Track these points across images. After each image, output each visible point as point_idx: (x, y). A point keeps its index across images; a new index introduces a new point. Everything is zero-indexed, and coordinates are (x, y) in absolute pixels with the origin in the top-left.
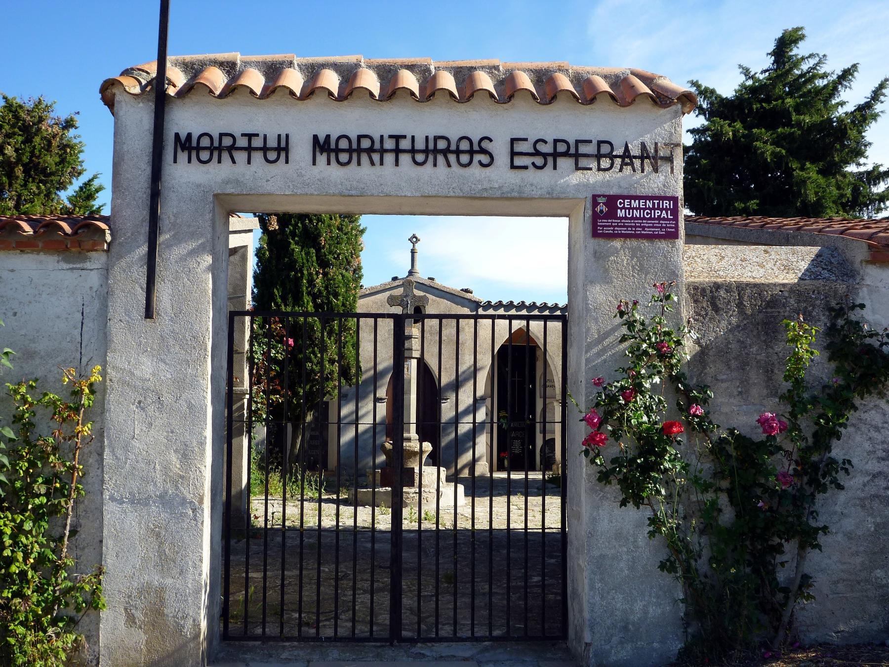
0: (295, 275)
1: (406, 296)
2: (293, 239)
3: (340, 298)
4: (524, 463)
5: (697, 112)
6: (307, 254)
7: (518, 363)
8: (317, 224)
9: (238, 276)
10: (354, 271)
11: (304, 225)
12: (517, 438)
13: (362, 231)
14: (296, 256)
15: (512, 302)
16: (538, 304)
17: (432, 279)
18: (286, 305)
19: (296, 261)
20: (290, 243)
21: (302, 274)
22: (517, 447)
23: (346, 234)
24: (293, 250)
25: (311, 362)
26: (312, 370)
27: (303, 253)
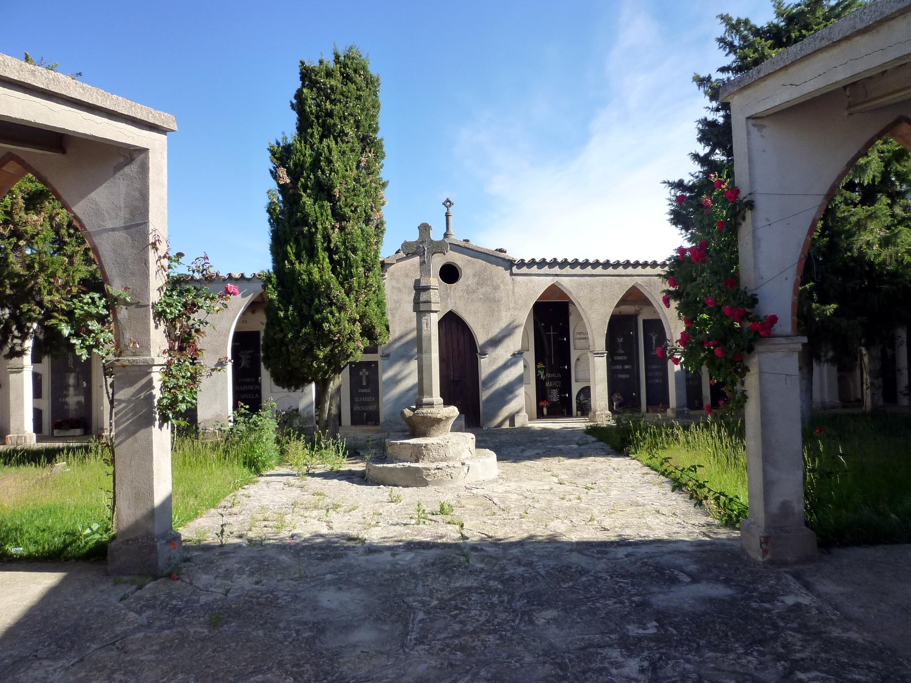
0: (309, 230)
1: (422, 242)
2: (305, 191)
3: (359, 253)
4: (561, 409)
5: (728, 50)
6: (321, 207)
7: (552, 318)
8: (330, 174)
9: (137, 194)
10: (377, 227)
11: (316, 177)
12: (554, 388)
13: (384, 185)
14: (308, 209)
15: (544, 260)
16: (570, 261)
17: (467, 241)
18: (300, 263)
19: (308, 215)
21: (317, 228)
22: (554, 396)
23: (364, 186)
24: (304, 203)
25: (328, 322)
26: (330, 331)
27: (317, 207)
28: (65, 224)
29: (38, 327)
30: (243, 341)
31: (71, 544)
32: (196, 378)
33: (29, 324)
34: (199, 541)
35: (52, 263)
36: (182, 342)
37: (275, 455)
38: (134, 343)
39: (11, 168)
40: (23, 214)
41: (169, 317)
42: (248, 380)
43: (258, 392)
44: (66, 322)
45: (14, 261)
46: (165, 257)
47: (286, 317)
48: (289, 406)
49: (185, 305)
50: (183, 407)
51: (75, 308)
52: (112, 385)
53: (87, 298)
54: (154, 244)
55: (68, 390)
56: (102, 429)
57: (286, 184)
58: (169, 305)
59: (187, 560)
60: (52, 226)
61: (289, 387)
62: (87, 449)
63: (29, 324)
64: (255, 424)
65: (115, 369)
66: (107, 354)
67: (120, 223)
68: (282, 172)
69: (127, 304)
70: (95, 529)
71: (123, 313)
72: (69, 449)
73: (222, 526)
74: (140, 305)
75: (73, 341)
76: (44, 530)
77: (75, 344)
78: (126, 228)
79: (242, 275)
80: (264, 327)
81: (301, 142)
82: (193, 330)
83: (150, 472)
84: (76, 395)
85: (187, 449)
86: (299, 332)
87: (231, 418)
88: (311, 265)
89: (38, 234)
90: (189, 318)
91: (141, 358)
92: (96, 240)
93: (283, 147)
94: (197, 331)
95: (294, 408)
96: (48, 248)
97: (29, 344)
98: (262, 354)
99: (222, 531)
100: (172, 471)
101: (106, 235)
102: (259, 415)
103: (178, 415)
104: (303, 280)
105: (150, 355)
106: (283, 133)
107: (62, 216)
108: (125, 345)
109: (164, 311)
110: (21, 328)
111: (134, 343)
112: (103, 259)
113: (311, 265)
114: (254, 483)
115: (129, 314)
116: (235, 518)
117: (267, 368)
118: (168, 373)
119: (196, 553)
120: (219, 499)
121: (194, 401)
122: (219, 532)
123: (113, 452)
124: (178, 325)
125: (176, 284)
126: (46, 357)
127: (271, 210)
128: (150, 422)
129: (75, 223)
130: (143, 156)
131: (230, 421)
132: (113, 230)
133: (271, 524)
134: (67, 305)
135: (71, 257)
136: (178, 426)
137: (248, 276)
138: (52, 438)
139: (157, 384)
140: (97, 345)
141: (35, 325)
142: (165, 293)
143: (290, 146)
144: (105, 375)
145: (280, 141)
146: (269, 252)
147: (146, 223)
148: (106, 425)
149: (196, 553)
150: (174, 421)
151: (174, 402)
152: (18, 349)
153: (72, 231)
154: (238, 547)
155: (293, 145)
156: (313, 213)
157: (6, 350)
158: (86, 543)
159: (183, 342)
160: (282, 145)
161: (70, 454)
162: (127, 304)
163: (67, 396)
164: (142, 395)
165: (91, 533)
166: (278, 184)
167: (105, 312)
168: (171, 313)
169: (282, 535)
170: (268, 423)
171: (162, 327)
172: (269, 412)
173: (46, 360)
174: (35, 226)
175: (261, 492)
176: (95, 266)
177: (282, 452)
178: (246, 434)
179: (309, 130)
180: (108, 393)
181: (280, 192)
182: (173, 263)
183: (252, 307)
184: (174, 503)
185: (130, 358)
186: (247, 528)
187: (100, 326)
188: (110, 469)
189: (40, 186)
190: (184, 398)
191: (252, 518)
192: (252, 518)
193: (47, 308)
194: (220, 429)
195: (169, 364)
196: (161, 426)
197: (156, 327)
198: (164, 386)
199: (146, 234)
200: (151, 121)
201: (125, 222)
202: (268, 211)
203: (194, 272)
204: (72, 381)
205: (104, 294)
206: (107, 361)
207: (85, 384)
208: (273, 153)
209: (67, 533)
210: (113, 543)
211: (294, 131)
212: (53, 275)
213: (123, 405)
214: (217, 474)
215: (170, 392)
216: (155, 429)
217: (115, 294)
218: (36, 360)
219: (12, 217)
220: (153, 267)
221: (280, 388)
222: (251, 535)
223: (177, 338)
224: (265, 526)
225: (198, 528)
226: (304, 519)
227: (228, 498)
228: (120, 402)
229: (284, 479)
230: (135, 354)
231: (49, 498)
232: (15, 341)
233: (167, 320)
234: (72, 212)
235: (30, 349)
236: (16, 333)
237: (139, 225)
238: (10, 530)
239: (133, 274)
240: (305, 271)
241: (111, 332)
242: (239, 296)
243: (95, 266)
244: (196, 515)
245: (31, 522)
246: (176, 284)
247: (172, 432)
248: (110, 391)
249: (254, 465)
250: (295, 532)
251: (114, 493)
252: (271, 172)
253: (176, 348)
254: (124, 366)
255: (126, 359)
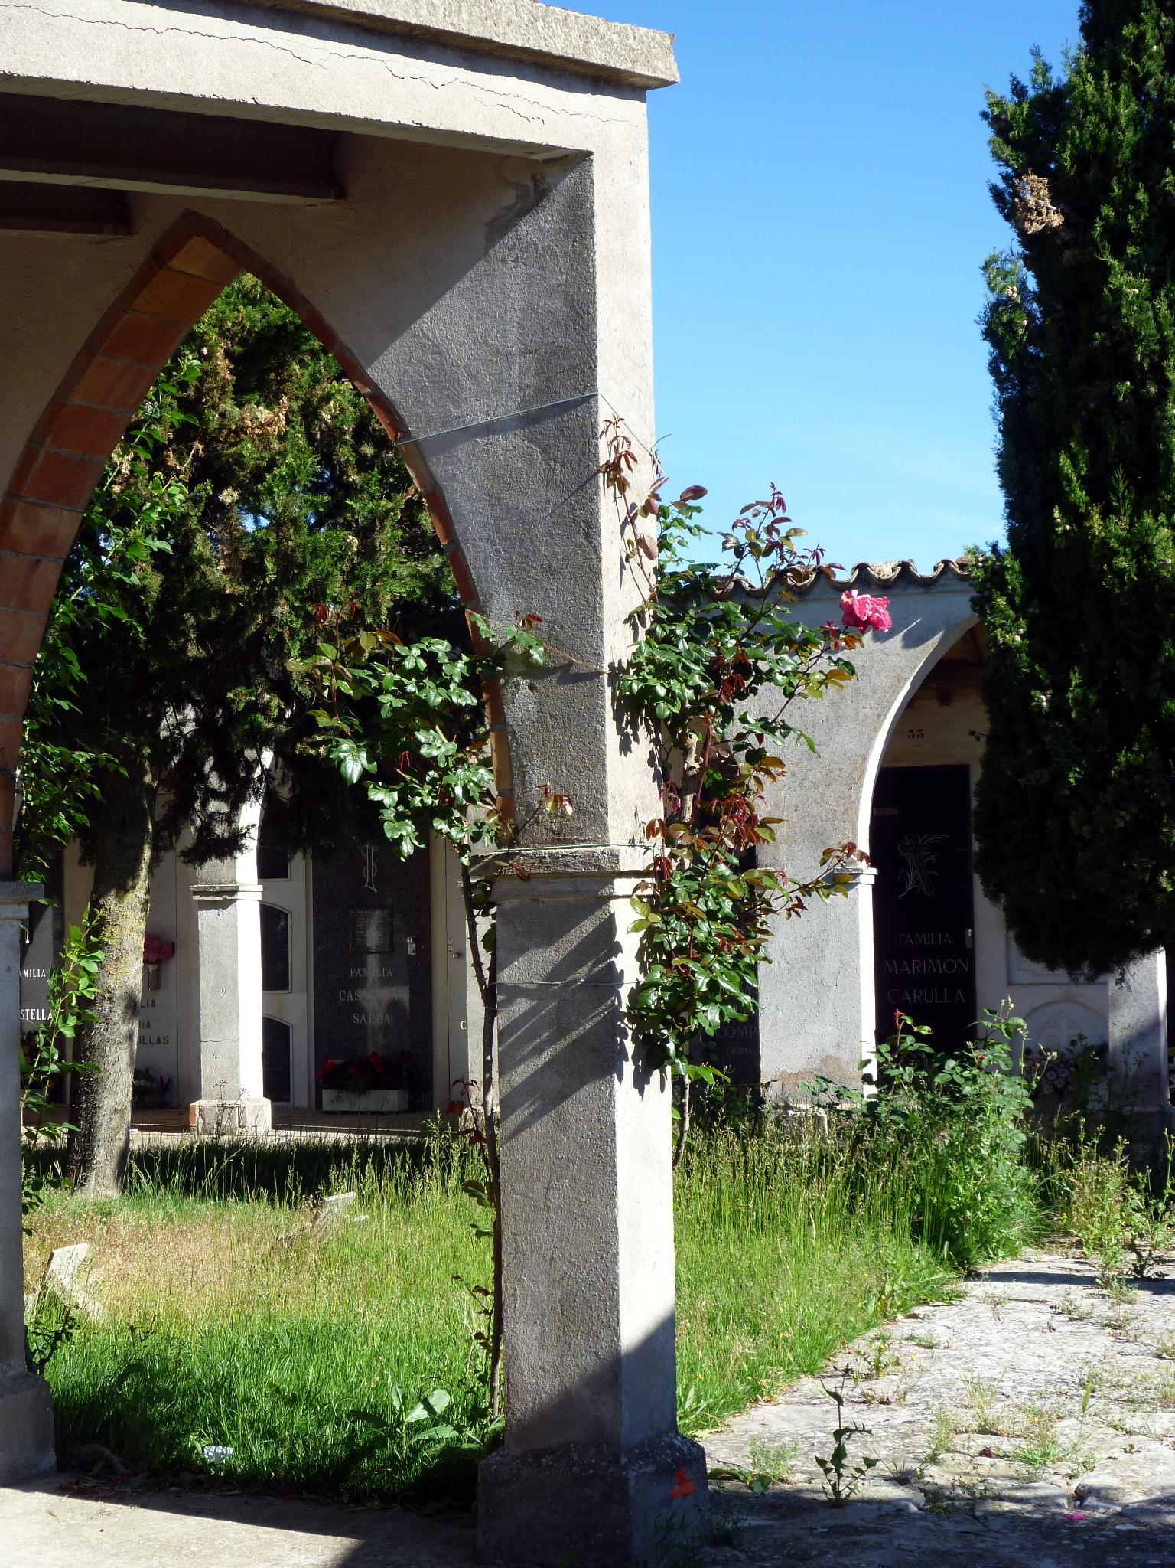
0: (1134, 392)
2: (1119, 253)
9: (558, 305)
14: (1130, 315)
18: (1105, 515)
19: (1132, 336)
20: (1107, 269)
24: (1118, 293)
28: (349, 427)
29: (275, 761)
30: (909, 798)
31: (368, 1450)
32: (752, 918)
33: (250, 754)
34: (763, 1480)
35: (315, 553)
36: (706, 795)
37: (1024, 1204)
38: (558, 799)
39: (195, 259)
40: (228, 405)
41: (664, 710)
42: (929, 939)
43: (966, 982)
44: (356, 737)
45: (208, 554)
46: (647, 509)
47: (1059, 707)
48: (1073, 1034)
49: (713, 671)
50: (710, 1016)
51: (380, 691)
52: (490, 941)
53: (413, 658)
54: (614, 468)
55: (363, 965)
56: (465, 1084)
57: (1048, 232)
58: (664, 671)
59: (725, 1539)
60: (310, 437)
61: (1072, 966)
62: (419, 1157)
63: (250, 754)
64: (952, 1090)
65: (502, 887)
66: (476, 837)
67: (508, 407)
68: (1035, 191)
69: (534, 672)
70: (439, 1409)
71: (522, 701)
72: (365, 1150)
73: (838, 1434)
74: (572, 673)
75: (377, 795)
76: (293, 1401)
77: (380, 805)
78: (528, 420)
79: (905, 566)
80: (981, 748)
81: (1098, 78)
82: (741, 757)
83: (606, 1233)
84: (385, 982)
85: (724, 1170)
86: (1112, 761)
87: (872, 1070)
88: (1148, 520)
89: (272, 464)
90: (727, 714)
91: (579, 850)
92: (440, 467)
93: (1038, 103)
94: (756, 757)
95: (1091, 1041)
96: (300, 506)
97: (251, 814)
98: (976, 846)
99: (839, 1454)
100: (678, 1242)
101: (467, 446)
102: (966, 1062)
103: (700, 1047)
104: (1120, 573)
105: (605, 841)
106: (1036, 53)
107: (340, 402)
108: (529, 807)
109: (648, 691)
110: (225, 769)
111: (558, 799)
112: (459, 529)
113: (1148, 520)
114: (950, 1298)
115: (538, 703)
116: (881, 1414)
117: (993, 895)
118: (662, 903)
119: (754, 1521)
120: (830, 1345)
121: (746, 999)
122: (827, 1457)
123: (493, 1161)
124: (694, 740)
125: (686, 597)
126: (299, 856)
127: (997, 329)
128: (610, 1066)
129: (380, 423)
130: (574, 175)
131: (867, 1079)
132: (488, 429)
133: (1006, 1445)
134: (357, 682)
135: (366, 533)
136: (699, 1082)
137: (924, 569)
138: (316, 1116)
139: (629, 941)
140: (446, 807)
141: (267, 757)
142: (651, 633)
143: (1060, 93)
144: (471, 904)
145: (1025, 80)
146: (996, 480)
147: (587, 400)
148: (476, 1072)
149: (754, 1521)
150: (683, 1067)
151: (683, 999)
152: (221, 830)
153: (368, 450)
154: (893, 1511)
155: (1070, 88)
156: (1149, 330)
157: (189, 835)
158: (415, 1450)
159: (711, 798)
160: (1031, 93)
161: (370, 1170)
162: (534, 672)
163: (360, 983)
164: (582, 974)
165: (429, 1413)
166: (1022, 233)
167: (468, 699)
168: (671, 696)
169: (1043, 1489)
170: (1004, 1098)
171: (644, 746)
172: (1000, 1050)
173: (299, 865)
174: (264, 439)
175: (971, 1334)
176: (437, 560)
177: (1049, 1197)
178: (920, 1124)
179: (1128, 31)
180: (478, 964)
181: (1030, 262)
182: (675, 531)
183: (937, 685)
184: (682, 1340)
185: (545, 851)
186: (923, 1452)
187: (452, 746)
188: (485, 1217)
189: (278, 312)
190: (713, 985)
191: (941, 1419)
192: (941, 1419)
193: (301, 699)
194: (831, 1107)
195: (660, 871)
196: (640, 1081)
197: (625, 747)
198: (652, 949)
199: (587, 439)
200: (597, 56)
201: (524, 403)
202: (989, 334)
203: (739, 552)
204: (373, 937)
205: (463, 639)
206: (475, 860)
207: (411, 947)
208: (1000, 124)
209: (357, 1414)
210: (495, 1458)
211: (1074, 40)
212: (318, 593)
213: (522, 1006)
214: (818, 1264)
215: (667, 964)
216: (623, 1088)
217: (498, 641)
218: (270, 868)
219: (200, 416)
220: (611, 546)
221: (1040, 968)
222: (938, 1476)
223: (689, 783)
224: (986, 1453)
225: (764, 1435)
226: (1123, 1440)
227: (860, 1344)
228: (515, 992)
229: (1053, 1293)
230: (558, 839)
231: (309, 1300)
232: (214, 806)
233: (657, 721)
234: (368, 382)
235: (255, 833)
236: (214, 780)
237: (565, 408)
238: (199, 1389)
239: (551, 572)
240: (1123, 542)
241: (486, 763)
242: (897, 640)
243: (437, 560)
244: (755, 1395)
245: (259, 1373)
246: (686, 597)
247: (678, 1106)
248: (486, 958)
249: (952, 1239)
250: (1092, 1480)
251: (498, 1294)
252: (997, 195)
253: (688, 816)
254: (525, 878)
255: (534, 851)
